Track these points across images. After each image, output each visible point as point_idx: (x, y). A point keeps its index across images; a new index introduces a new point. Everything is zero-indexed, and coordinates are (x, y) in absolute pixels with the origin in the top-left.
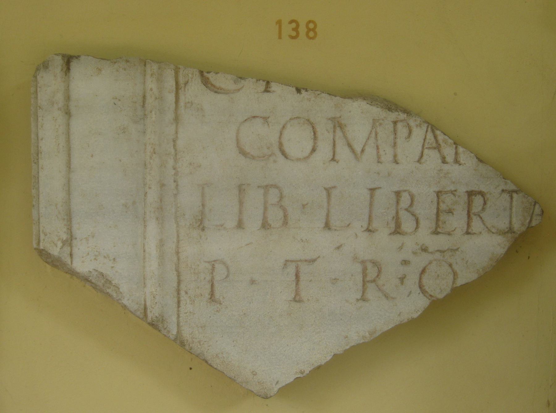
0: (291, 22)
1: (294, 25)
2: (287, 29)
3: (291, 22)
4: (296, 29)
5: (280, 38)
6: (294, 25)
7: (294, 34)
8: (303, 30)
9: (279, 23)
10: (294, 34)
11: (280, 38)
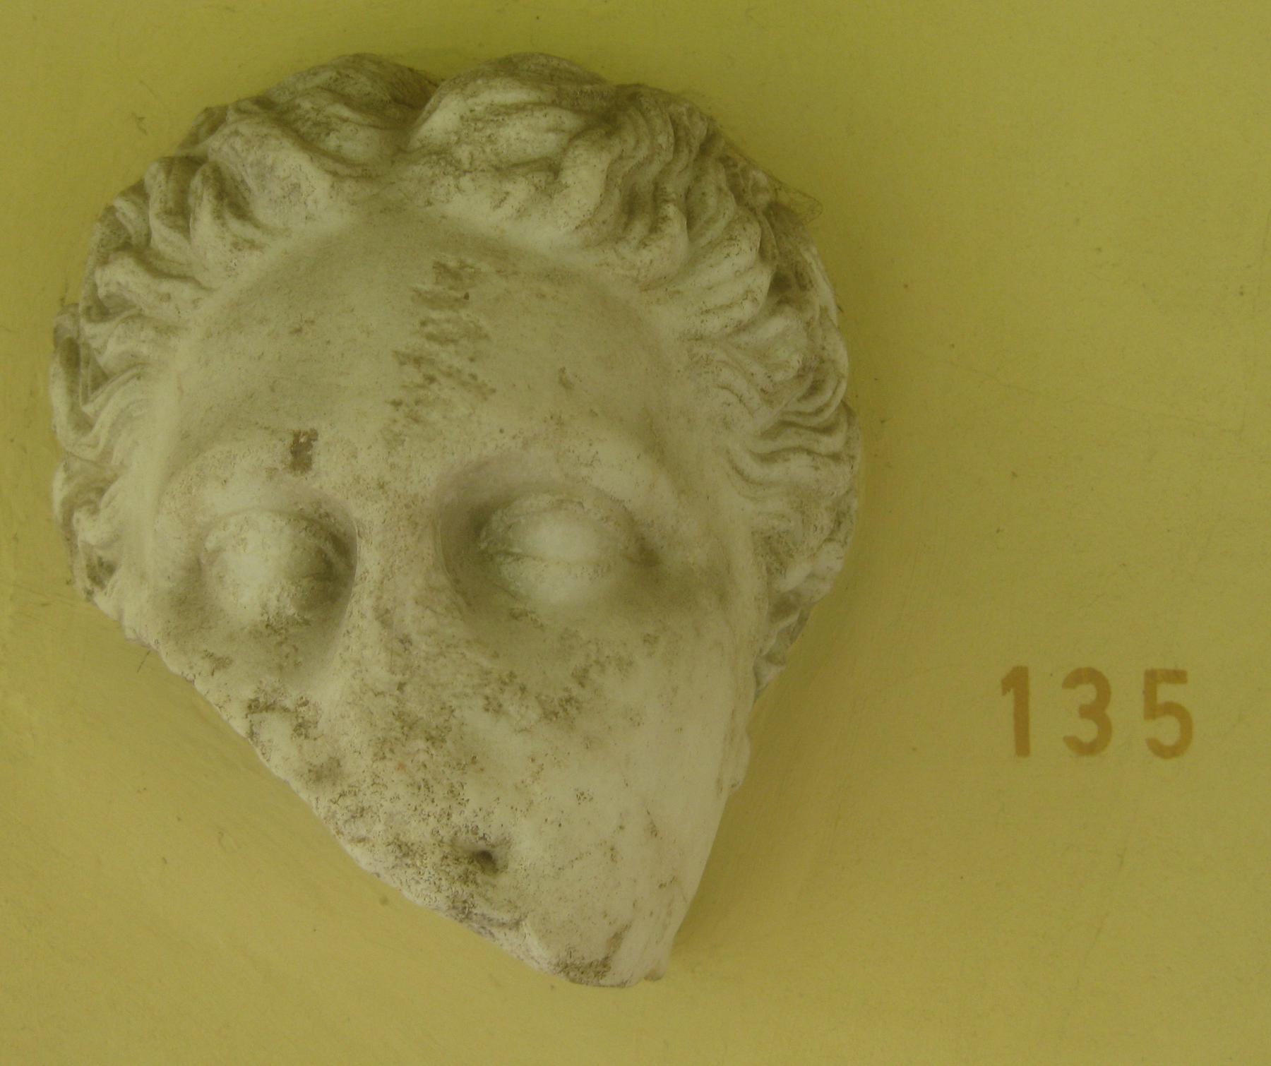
0: (1077, 678)
1: (1087, 693)
2: (1056, 715)
3: (1077, 678)
4: (1096, 712)
5: (1022, 745)
6: (1087, 693)
7: (1088, 731)
8: (1126, 706)
9: (1017, 682)
10: (1088, 731)
11: (1022, 745)
